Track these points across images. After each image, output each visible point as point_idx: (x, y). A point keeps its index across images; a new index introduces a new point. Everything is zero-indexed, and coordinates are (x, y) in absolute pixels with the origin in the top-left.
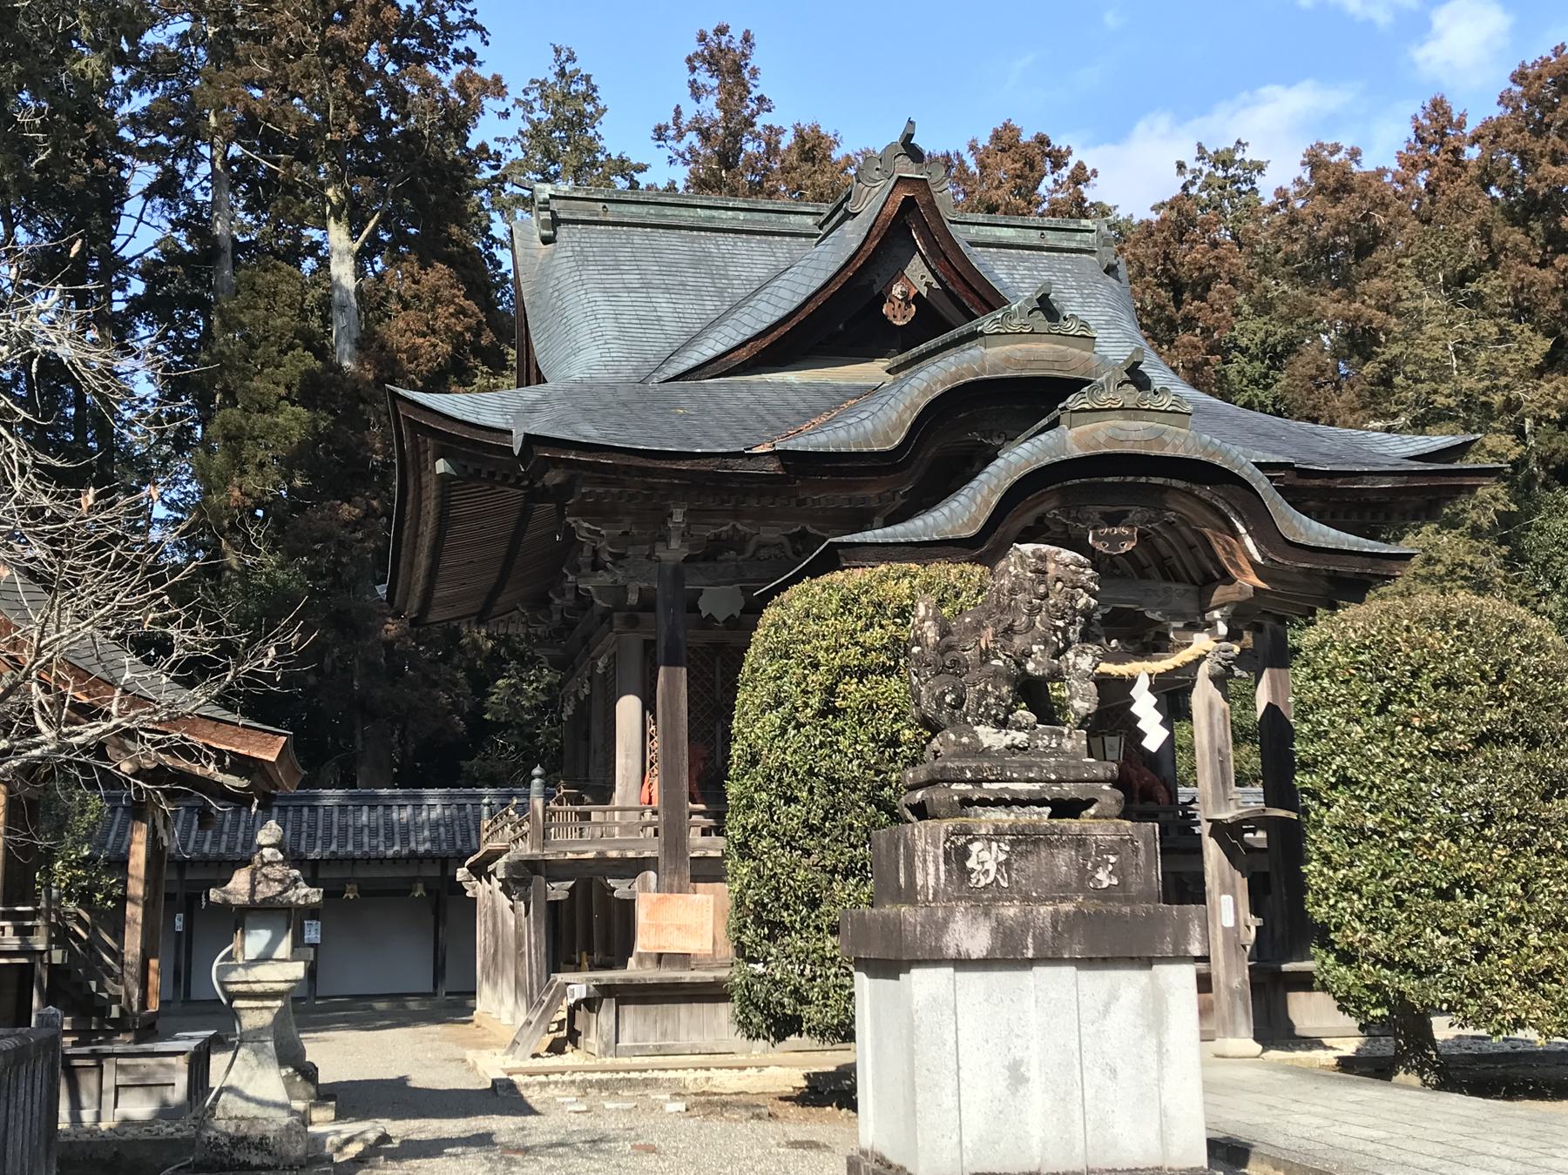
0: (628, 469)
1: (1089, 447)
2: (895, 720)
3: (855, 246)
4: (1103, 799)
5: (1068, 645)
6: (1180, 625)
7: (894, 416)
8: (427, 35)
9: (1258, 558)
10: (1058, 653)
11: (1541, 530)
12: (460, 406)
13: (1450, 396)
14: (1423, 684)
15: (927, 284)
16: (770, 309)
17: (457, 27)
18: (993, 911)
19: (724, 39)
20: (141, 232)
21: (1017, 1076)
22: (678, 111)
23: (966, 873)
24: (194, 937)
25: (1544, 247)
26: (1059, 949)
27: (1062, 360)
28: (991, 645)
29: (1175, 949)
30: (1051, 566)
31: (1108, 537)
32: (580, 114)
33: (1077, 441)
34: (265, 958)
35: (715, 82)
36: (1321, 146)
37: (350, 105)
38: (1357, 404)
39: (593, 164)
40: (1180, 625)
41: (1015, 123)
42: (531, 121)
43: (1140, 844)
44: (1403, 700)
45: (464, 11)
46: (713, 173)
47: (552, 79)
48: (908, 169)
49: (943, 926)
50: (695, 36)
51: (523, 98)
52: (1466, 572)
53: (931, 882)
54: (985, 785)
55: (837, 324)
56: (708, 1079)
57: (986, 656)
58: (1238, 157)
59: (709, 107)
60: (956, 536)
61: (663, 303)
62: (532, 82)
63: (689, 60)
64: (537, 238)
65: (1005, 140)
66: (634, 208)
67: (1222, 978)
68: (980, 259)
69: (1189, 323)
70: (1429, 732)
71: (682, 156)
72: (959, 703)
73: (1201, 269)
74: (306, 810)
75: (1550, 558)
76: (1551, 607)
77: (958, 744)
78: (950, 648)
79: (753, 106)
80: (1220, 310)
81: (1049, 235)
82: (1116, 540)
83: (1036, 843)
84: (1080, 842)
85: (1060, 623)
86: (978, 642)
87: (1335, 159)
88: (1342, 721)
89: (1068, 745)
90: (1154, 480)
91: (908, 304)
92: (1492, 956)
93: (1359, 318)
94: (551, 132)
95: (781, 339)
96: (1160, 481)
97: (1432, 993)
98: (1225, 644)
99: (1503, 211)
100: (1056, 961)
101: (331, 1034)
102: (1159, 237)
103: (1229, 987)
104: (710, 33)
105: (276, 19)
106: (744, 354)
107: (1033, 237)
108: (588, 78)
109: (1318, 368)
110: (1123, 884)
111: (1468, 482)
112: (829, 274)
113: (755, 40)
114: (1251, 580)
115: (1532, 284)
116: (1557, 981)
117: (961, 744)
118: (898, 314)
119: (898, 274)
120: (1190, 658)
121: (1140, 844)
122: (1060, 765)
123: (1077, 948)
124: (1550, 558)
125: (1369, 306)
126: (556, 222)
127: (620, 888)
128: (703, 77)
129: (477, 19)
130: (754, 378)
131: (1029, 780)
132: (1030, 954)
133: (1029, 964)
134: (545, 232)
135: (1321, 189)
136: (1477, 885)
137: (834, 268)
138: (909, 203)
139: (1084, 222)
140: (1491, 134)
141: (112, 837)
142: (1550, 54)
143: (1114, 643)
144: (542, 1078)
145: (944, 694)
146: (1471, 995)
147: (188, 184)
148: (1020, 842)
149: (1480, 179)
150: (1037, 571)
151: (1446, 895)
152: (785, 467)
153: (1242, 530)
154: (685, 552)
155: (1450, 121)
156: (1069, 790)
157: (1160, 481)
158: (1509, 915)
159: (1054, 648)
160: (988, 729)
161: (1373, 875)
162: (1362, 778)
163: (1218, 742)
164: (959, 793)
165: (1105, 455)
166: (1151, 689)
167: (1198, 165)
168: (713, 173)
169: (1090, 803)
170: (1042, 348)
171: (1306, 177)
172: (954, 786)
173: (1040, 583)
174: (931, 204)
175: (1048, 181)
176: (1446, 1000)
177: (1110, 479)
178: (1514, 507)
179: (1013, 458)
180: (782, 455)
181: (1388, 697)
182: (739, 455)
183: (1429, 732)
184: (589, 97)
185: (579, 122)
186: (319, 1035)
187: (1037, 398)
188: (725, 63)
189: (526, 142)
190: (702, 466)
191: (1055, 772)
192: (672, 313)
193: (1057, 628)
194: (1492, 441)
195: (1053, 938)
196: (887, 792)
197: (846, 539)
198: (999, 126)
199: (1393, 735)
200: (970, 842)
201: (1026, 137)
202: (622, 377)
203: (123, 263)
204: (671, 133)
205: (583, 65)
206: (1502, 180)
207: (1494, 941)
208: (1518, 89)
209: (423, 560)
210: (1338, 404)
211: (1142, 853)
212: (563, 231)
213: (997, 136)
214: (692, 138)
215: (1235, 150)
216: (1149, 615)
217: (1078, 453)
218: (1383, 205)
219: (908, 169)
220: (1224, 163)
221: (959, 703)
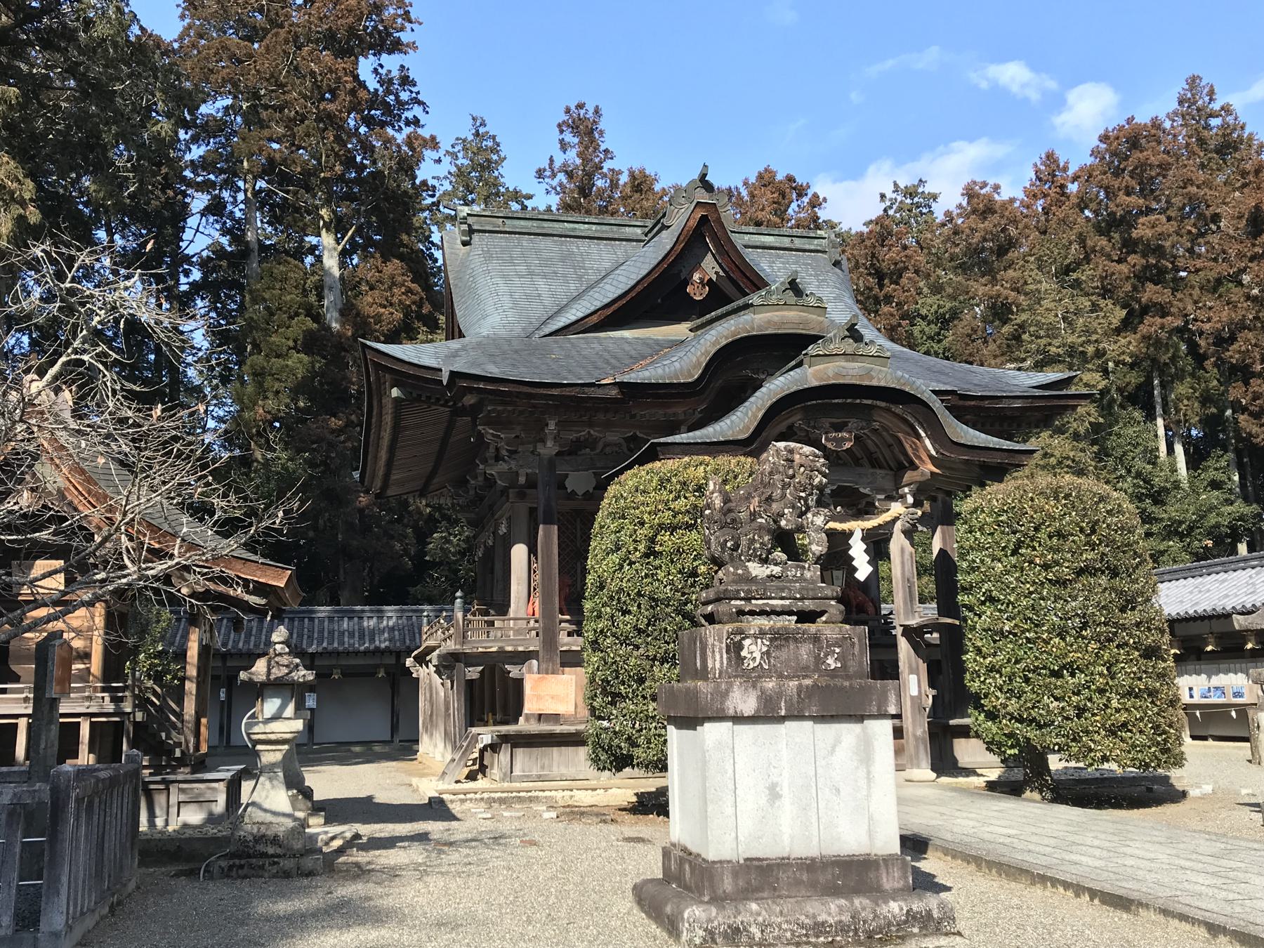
0: (530, 396)
1: (822, 379)
2: (695, 560)
3: (668, 248)
5: (808, 509)
7: (694, 359)
9: (933, 453)
10: (802, 514)
11: (1119, 435)
14: (1042, 535)
16: (613, 289)
17: (407, 103)
19: (582, 112)
20: (200, 238)
21: (774, 793)
22: (551, 160)
25: (1120, 250)
27: (804, 322)
29: (879, 709)
30: (797, 457)
31: (835, 439)
32: (489, 161)
33: (814, 375)
34: (277, 717)
35: (576, 140)
36: (975, 183)
37: (337, 155)
42: (456, 165)
43: (856, 640)
44: (1029, 546)
47: (470, 138)
48: (703, 196)
49: (725, 695)
51: (451, 150)
52: (1069, 462)
53: (718, 666)
55: (657, 299)
56: (572, 797)
57: (754, 516)
58: (920, 190)
59: (572, 157)
61: (541, 284)
62: (457, 139)
63: (559, 126)
64: (459, 242)
65: (765, 178)
66: (522, 223)
67: (910, 729)
69: (888, 299)
70: (1046, 567)
71: (555, 189)
72: (736, 547)
73: (896, 264)
75: (1125, 454)
76: (1126, 485)
77: (735, 574)
78: (730, 511)
81: (797, 241)
83: (787, 639)
84: (816, 639)
85: (803, 494)
87: (983, 191)
89: (808, 575)
90: (865, 402)
91: (704, 286)
93: (999, 296)
96: (869, 402)
97: (1048, 739)
100: (800, 717)
102: (868, 243)
103: (914, 735)
104: (573, 108)
105: (287, 97)
106: (595, 319)
107: (786, 242)
108: (494, 137)
110: (844, 666)
113: (602, 112)
115: (1113, 274)
116: (1130, 731)
118: (697, 293)
119: (697, 266)
121: (856, 640)
122: (802, 588)
124: (1125, 454)
126: (471, 231)
127: (514, 671)
128: (569, 137)
130: (602, 335)
131: (783, 598)
133: (782, 719)
135: (974, 211)
136: (1078, 668)
137: (655, 262)
138: (704, 219)
140: (1086, 175)
143: (839, 509)
144: (462, 796)
145: (726, 541)
146: (1074, 740)
147: (229, 207)
148: (776, 639)
151: (1057, 674)
152: (623, 393)
153: (923, 434)
154: (556, 449)
156: (809, 605)
157: (869, 402)
163: (907, 574)
164: (736, 607)
167: (894, 196)
169: (822, 613)
170: (792, 315)
171: (965, 203)
175: (794, 206)
179: (772, 387)
180: (621, 385)
183: (1046, 567)
184: (495, 150)
185: (488, 166)
188: (583, 127)
190: (567, 392)
192: (548, 292)
193: (801, 498)
194: (1087, 377)
196: (689, 607)
197: (662, 440)
198: (762, 169)
199: (1022, 569)
200: (743, 639)
203: (188, 259)
204: (548, 173)
205: (491, 129)
207: (1089, 704)
209: (383, 455)
211: (857, 646)
213: (760, 177)
214: (561, 177)
215: (919, 185)
216: (862, 490)
217: (815, 383)
218: (1014, 222)
219: (703, 196)
221: (736, 547)
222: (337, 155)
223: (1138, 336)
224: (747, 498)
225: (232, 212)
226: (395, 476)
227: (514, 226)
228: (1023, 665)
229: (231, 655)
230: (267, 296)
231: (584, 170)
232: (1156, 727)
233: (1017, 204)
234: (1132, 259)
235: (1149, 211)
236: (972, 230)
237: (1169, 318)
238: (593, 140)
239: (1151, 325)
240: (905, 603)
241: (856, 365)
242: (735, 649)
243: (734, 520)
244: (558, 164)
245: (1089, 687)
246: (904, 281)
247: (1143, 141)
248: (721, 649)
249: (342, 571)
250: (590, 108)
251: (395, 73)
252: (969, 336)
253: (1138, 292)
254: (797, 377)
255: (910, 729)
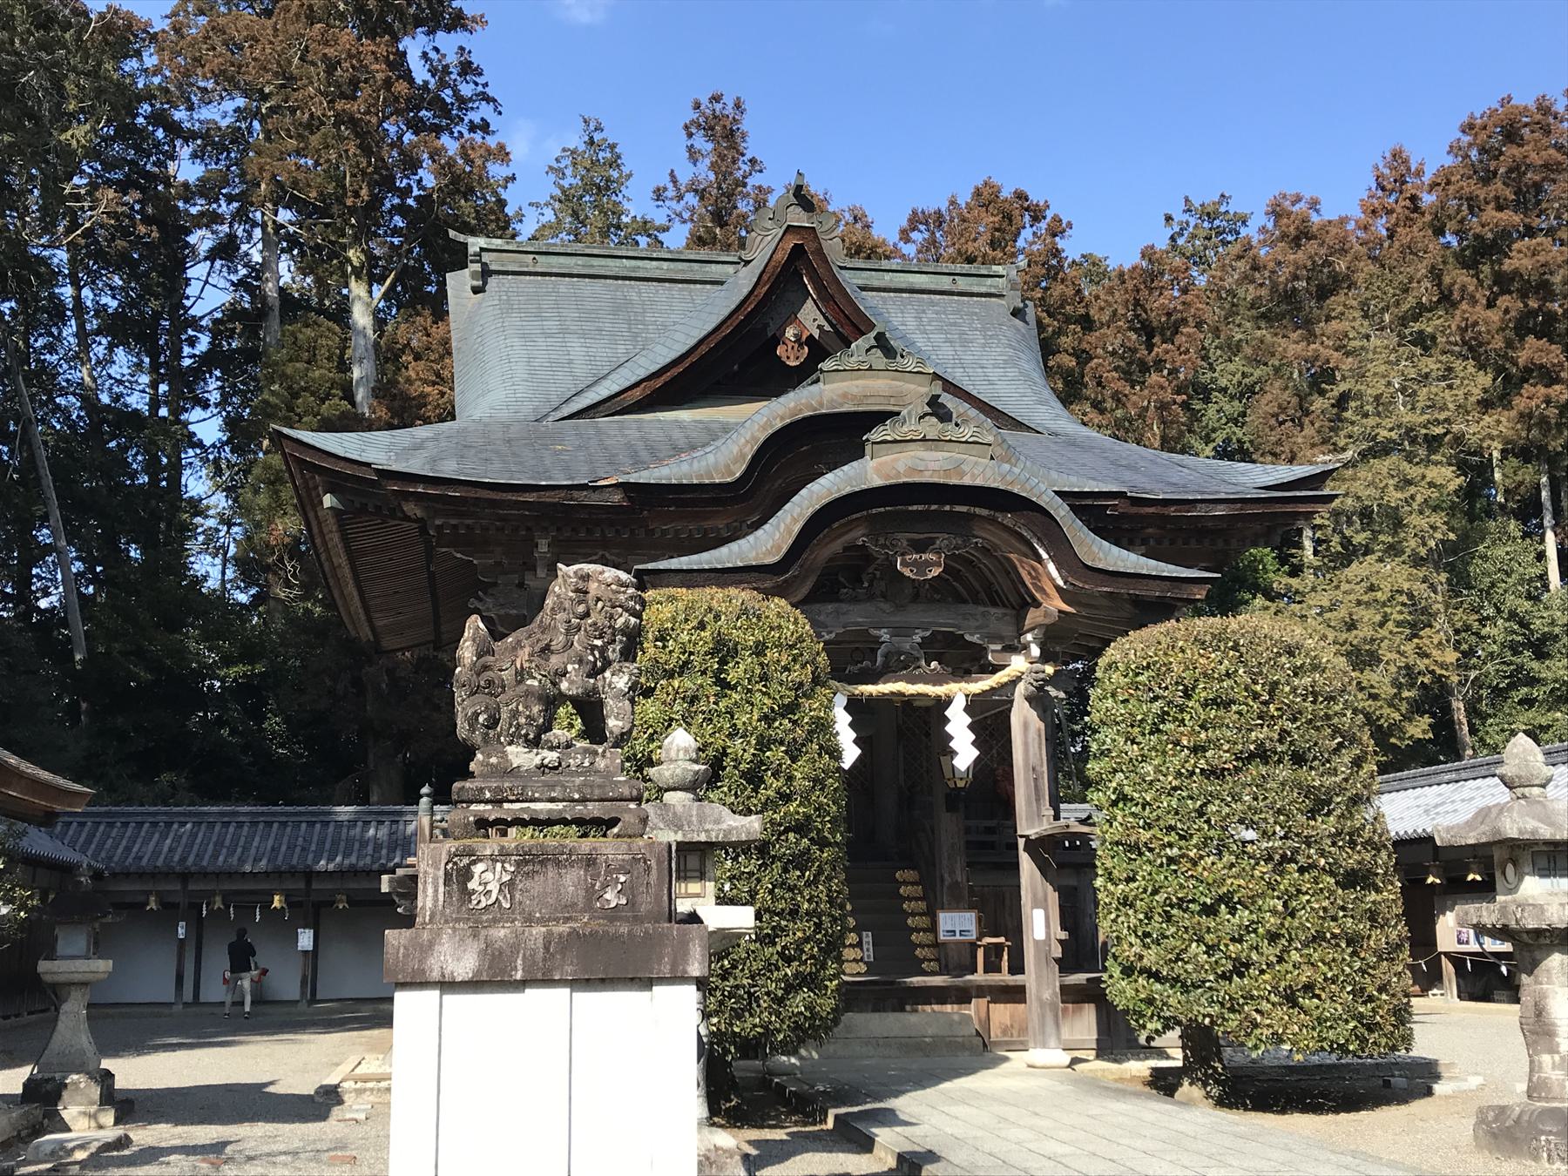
0: (493, 503)
1: (888, 477)
3: (745, 291)
4: (626, 817)
5: (607, 663)
6: (999, 647)
7: (735, 450)
8: (443, 109)
9: (1060, 583)
10: (595, 672)
11: (1484, 558)
12: (346, 444)
13: (1391, 430)
15: (819, 327)
17: (471, 99)
18: (483, 933)
20: (209, 293)
22: (672, 174)
23: (467, 894)
24: (204, 950)
26: (550, 971)
28: (526, 665)
30: (593, 587)
31: (915, 563)
33: (877, 470)
35: (710, 146)
36: (1284, 196)
37: (364, 173)
38: (1317, 439)
39: (618, 227)
40: (999, 647)
41: (995, 180)
42: (562, 188)
43: (653, 863)
44: (1175, 719)
45: (476, 84)
46: (709, 230)
47: (582, 147)
48: (798, 217)
50: (691, 105)
51: (555, 165)
52: (1404, 598)
53: (429, 904)
54: (506, 805)
55: (732, 362)
57: (521, 675)
58: (1222, 209)
59: (704, 172)
60: (760, 562)
61: (576, 348)
62: (564, 150)
65: (986, 197)
66: (562, 259)
67: (1034, 991)
68: (869, 303)
69: (1159, 364)
70: (1197, 750)
71: (680, 215)
72: (493, 722)
73: (1169, 315)
74: (304, 826)
75: (1493, 585)
76: (1495, 631)
78: (486, 668)
79: (747, 168)
80: (1187, 352)
82: (922, 566)
85: (598, 643)
86: (513, 662)
87: (1296, 208)
88: (1121, 740)
89: (601, 764)
90: (958, 508)
91: (801, 345)
92: (1253, 972)
93: (1317, 358)
94: (582, 197)
95: (673, 379)
96: (964, 509)
97: (1196, 1008)
98: (1038, 666)
99: (1455, 254)
100: (547, 982)
101: (305, 1037)
102: (1130, 285)
103: (1040, 999)
104: (704, 101)
105: (300, 95)
106: (637, 394)
107: (945, 283)
108: (612, 147)
109: (1280, 406)
111: (1302, 508)
112: (721, 318)
114: (1056, 604)
115: (1476, 324)
116: (1318, 997)
117: (488, 764)
119: (792, 317)
120: (1005, 680)
121: (653, 863)
122: (584, 784)
123: (569, 969)
124: (1493, 585)
125: (1327, 347)
126: (486, 273)
128: (701, 143)
129: (490, 91)
131: (552, 800)
132: (519, 976)
134: (476, 283)
135: (1284, 236)
136: (1239, 902)
137: (726, 312)
138: (798, 251)
139: (995, 268)
140: (1442, 182)
141: (120, 851)
142: (1497, 106)
143: (934, 664)
146: (1232, 1010)
147: (244, 247)
148: (527, 862)
149: (1431, 225)
150: (577, 591)
151: (1210, 911)
153: (1045, 556)
155: (1409, 169)
156: (593, 809)
157: (964, 509)
158: (1268, 931)
159: (589, 667)
160: (520, 749)
161: (1145, 891)
162: (1136, 795)
163: (1033, 760)
165: (905, 484)
166: (967, 710)
167: (1186, 217)
168: (709, 230)
169: (613, 822)
171: (1270, 226)
172: (473, 807)
173: (580, 603)
174: (819, 251)
175: (1027, 234)
176: (1209, 1015)
177: (915, 508)
178: (1452, 536)
181: (1163, 717)
182: (584, 487)
183: (1197, 750)
184: (614, 163)
185: (605, 188)
186: (298, 1037)
187: (843, 434)
188: (720, 130)
189: (557, 205)
190: (548, 498)
191: (579, 791)
193: (594, 647)
194: (1433, 473)
195: (545, 960)
197: (650, 566)
198: (980, 184)
199: (1164, 753)
200: (474, 863)
201: (1006, 193)
202: (520, 416)
203: (194, 323)
204: (671, 193)
206: (1451, 225)
207: (1255, 956)
208: (1466, 139)
209: (351, 588)
210: (1300, 440)
211: (654, 872)
212: (493, 281)
213: (978, 193)
214: (691, 199)
215: (1220, 203)
216: (967, 637)
219: (798, 217)
220: (1208, 214)
221: (493, 722)
222: (364, 173)
223: (1513, 413)
224: (514, 649)
225: (247, 254)
226: (443, 628)
227: (521, 264)
228: (1160, 898)
229: (192, 874)
230: (289, 371)
231: (719, 188)
232: (1358, 992)
233: (1351, 226)
234: (1504, 301)
235: (1530, 232)
236: (1279, 263)
237: (1557, 387)
238: (734, 146)
239: (1532, 397)
240: (1028, 803)
241: (940, 455)
242: (459, 878)
243: (490, 683)
244: (684, 179)
245: (1255, 931)
246: (1179, 339)
247: (1526, 131)
248: (435, 879)
249: (371, 756)
250: (729, 100)
251: (452, 59)
252: (1275, 416)
253: (1514, 349)
254: (852, 473)
255: (1034, 991)
